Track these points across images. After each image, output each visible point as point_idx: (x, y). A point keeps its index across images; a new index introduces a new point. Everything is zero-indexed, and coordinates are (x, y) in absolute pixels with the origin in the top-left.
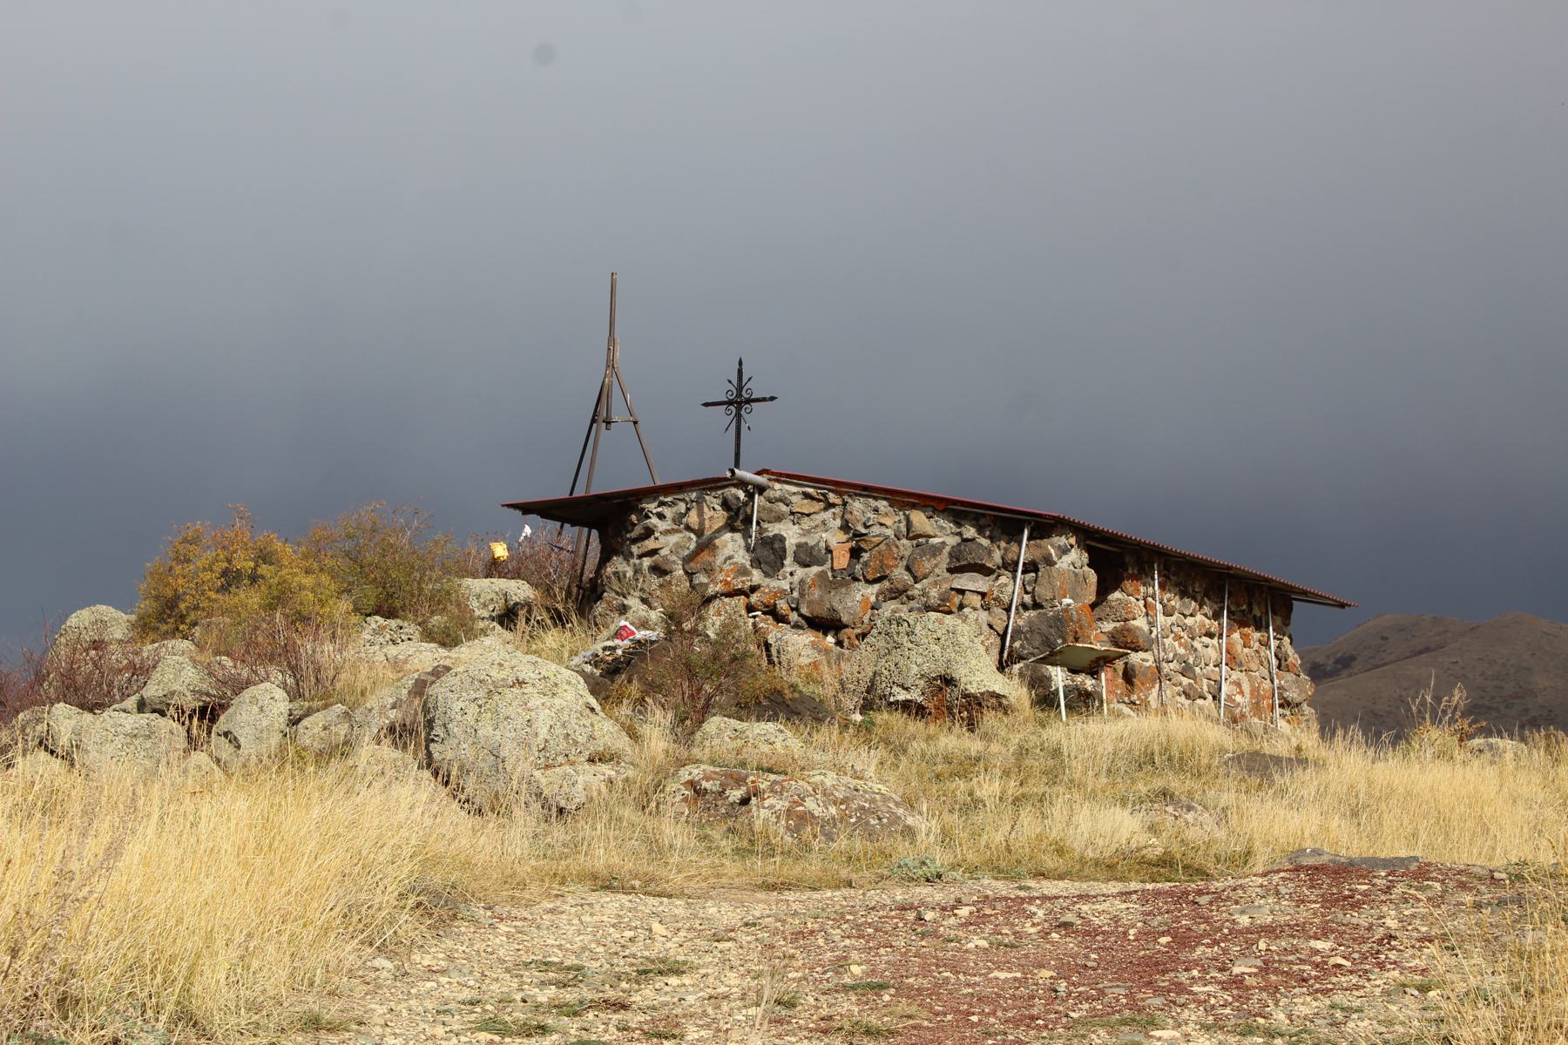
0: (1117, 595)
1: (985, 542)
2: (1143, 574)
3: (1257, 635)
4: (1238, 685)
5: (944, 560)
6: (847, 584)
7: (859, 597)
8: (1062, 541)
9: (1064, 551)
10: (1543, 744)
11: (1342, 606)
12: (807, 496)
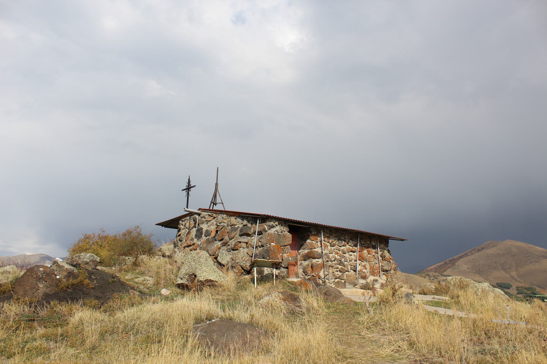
0: (308, 241)
1: (249, 225)
2: (318, 234)
4: (364, 266)
5: (238, 232)
6: (212, 242)
7: (216, 246)
8: (271, 223)
9: (273, 227)
10: (227, 353)
11: (403, 240)
12: (209, 215)
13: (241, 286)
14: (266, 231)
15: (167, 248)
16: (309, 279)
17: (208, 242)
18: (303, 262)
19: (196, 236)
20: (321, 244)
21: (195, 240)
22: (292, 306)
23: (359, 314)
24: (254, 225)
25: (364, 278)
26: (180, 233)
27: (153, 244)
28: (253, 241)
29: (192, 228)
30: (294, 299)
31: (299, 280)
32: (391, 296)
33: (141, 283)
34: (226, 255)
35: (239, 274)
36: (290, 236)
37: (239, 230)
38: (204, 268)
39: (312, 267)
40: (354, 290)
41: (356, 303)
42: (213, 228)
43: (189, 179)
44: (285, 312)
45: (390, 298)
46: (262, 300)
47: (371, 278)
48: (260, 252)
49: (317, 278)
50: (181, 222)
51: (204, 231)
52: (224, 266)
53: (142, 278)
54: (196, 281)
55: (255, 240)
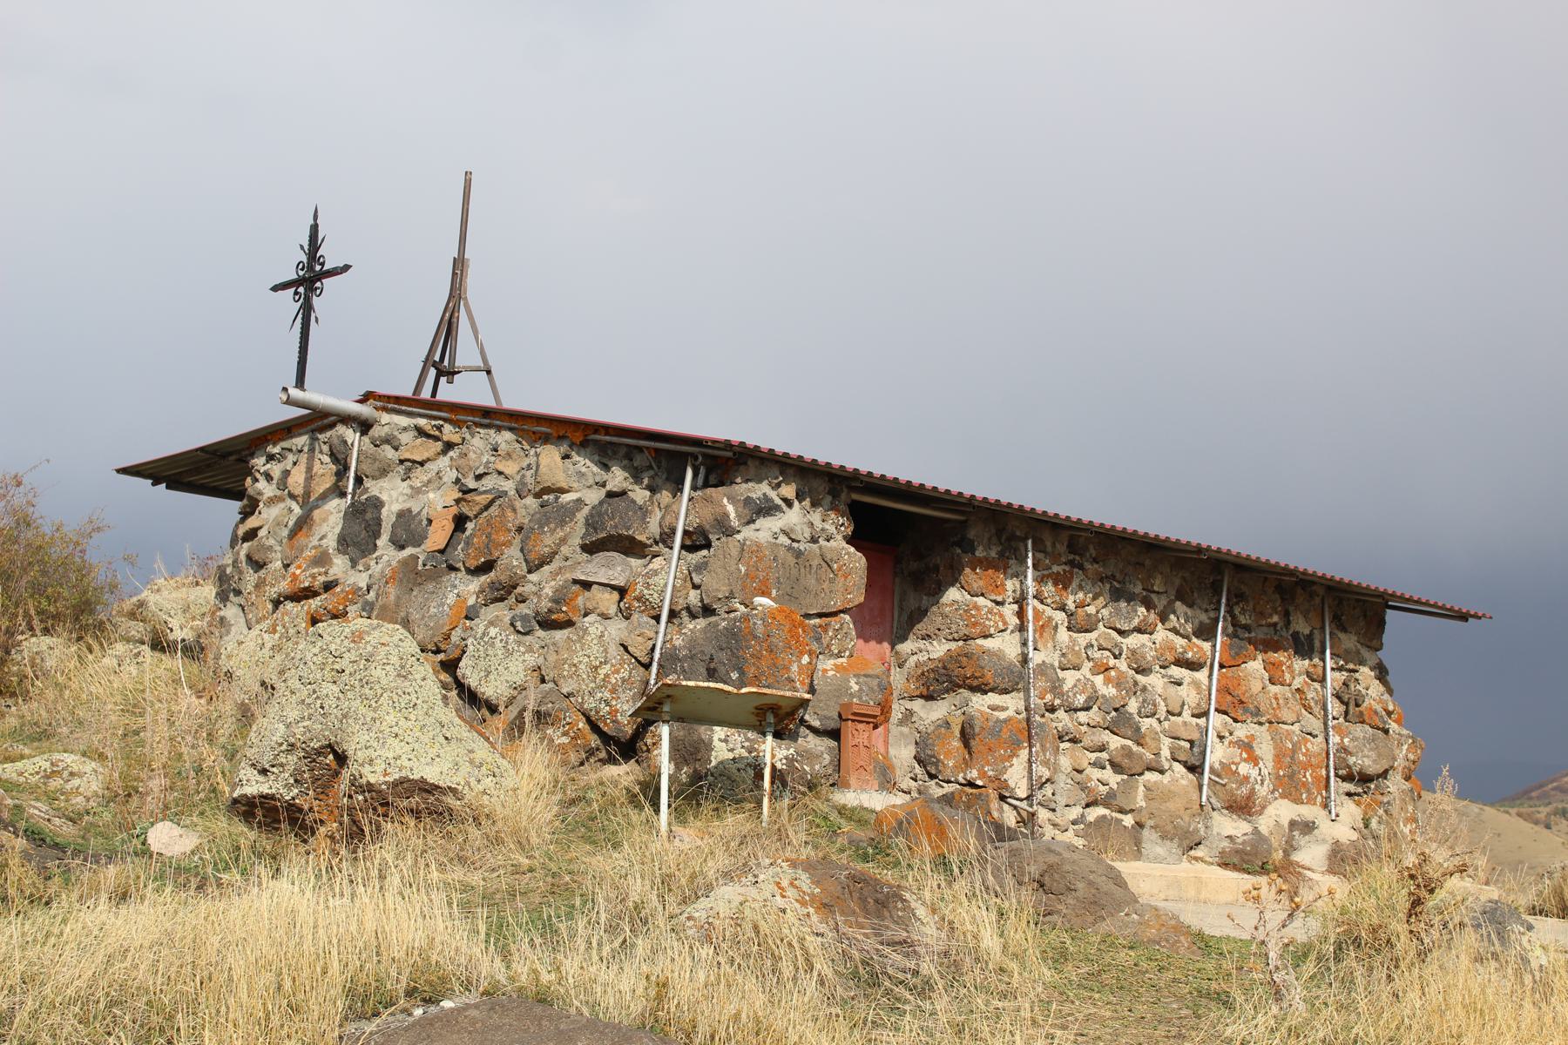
0: (953, 594)
1: (640, 495)
2: (1007, 559)
3: (1301, 664)
4: (1247, 746)
5: (577, 531)
6: (434, 575)
7: (451, 599)
9: (766, 509)
11: (1464, 617)
12: (421, 432)
13: (586, 823)
14: (730, 532)
15: (178, 601)
16: (947, 800)
17: (411, 576)
18: (917, 705)
19: (344, 542)
20: (1021, 614)
21: (339, 566)
22: (864, 940)
23: (1226, 1002)
24: (665, 496)
25: (1243, 807)
26: (252, 522)
27: (100, 576)
28: (658, 580)
29: (324, 497)
30: (880, 903)
31: (899, 799)
32: (1402, 916)
33: (33, 790)
34: (509, 653)
35: (574, 758)
36: (856, 561)
37: (581, 516)
38: (390, 719)
39: (966, 737)
40: (1185, 869)
41: (1204, 943)
42: (438, 502)
43: (314, 229)
44: (828, 972)
45: (1399, 927)
46: (703, 903)
47: (1280, 812)
48: (692, 643)
49: (993, 795)
50: (259, 462)
51: (388, 514)
52: (493, 709)
53: (42, 763)
54: (343, 785)
55: (666, 574)
